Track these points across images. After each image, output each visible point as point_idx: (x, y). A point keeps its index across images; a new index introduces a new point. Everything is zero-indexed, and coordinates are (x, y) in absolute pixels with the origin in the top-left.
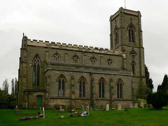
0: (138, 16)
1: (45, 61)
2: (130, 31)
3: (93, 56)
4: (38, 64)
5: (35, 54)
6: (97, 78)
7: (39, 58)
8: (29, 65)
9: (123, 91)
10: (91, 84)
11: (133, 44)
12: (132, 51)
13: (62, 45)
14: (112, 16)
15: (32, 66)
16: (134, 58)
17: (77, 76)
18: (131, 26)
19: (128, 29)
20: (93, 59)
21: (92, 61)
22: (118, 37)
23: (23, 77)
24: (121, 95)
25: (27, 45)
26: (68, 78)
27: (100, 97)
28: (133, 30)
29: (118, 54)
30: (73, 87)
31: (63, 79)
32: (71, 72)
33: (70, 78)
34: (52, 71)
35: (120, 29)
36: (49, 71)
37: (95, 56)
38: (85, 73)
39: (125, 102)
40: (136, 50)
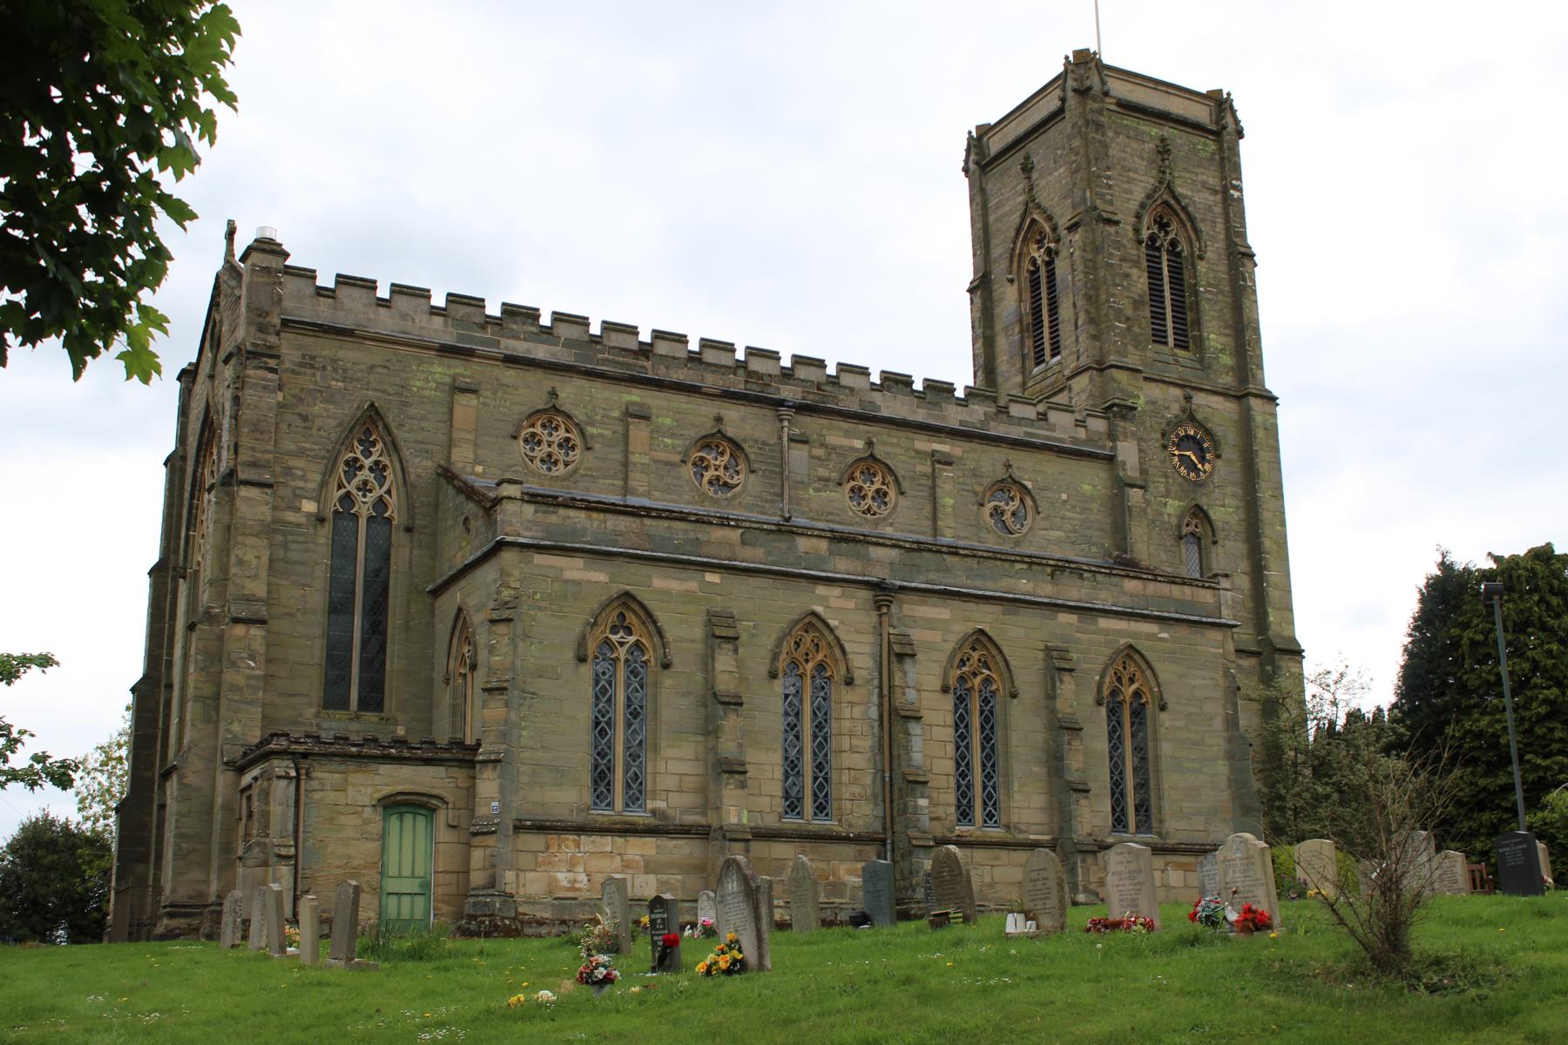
0: (1218, 134)
1: (447, 474)
2: (1158, 249)
3: (870, 444)
4: (380, 504)
5: (347, 411)
6: (936, 628)
7: (393, 447)
8: (298, 510)
9: (1157, 757)
10: (886, 692)
11: (1189, 364)
12: (1180, 424)
13: (595, 340)
14: (985, 131)
15: (322, 520)
16: (1198, 485)
17: (766, 611)
18: (1167, 209)
19: (1145, 234)
20: (870, 475)
21: (857, 492)
22: (1044, 302)
23: (236, 621)
24: (1143, 807)
25: (285, 323)
26: (684, 631)
27: (965, 814)
28: (1183, 247)
29: (1075, 440)
30: (731, 723)
31: (637, 644)
32: (712, 577)
33: (698, 632)
34: (540, 559)
35: (1072, 228)
36: (508, 557)
37: (891, 446)
38: (837, 591)
39: (1179, 866)
40: (1217, 410)
